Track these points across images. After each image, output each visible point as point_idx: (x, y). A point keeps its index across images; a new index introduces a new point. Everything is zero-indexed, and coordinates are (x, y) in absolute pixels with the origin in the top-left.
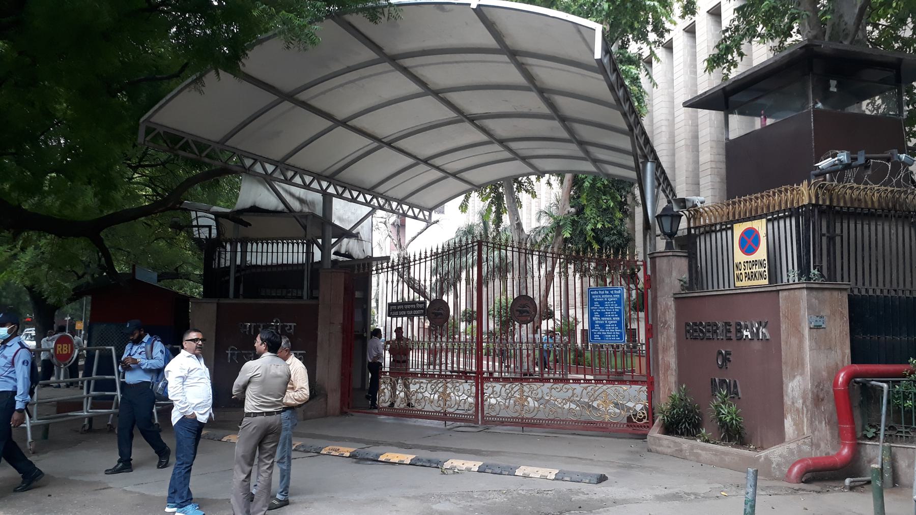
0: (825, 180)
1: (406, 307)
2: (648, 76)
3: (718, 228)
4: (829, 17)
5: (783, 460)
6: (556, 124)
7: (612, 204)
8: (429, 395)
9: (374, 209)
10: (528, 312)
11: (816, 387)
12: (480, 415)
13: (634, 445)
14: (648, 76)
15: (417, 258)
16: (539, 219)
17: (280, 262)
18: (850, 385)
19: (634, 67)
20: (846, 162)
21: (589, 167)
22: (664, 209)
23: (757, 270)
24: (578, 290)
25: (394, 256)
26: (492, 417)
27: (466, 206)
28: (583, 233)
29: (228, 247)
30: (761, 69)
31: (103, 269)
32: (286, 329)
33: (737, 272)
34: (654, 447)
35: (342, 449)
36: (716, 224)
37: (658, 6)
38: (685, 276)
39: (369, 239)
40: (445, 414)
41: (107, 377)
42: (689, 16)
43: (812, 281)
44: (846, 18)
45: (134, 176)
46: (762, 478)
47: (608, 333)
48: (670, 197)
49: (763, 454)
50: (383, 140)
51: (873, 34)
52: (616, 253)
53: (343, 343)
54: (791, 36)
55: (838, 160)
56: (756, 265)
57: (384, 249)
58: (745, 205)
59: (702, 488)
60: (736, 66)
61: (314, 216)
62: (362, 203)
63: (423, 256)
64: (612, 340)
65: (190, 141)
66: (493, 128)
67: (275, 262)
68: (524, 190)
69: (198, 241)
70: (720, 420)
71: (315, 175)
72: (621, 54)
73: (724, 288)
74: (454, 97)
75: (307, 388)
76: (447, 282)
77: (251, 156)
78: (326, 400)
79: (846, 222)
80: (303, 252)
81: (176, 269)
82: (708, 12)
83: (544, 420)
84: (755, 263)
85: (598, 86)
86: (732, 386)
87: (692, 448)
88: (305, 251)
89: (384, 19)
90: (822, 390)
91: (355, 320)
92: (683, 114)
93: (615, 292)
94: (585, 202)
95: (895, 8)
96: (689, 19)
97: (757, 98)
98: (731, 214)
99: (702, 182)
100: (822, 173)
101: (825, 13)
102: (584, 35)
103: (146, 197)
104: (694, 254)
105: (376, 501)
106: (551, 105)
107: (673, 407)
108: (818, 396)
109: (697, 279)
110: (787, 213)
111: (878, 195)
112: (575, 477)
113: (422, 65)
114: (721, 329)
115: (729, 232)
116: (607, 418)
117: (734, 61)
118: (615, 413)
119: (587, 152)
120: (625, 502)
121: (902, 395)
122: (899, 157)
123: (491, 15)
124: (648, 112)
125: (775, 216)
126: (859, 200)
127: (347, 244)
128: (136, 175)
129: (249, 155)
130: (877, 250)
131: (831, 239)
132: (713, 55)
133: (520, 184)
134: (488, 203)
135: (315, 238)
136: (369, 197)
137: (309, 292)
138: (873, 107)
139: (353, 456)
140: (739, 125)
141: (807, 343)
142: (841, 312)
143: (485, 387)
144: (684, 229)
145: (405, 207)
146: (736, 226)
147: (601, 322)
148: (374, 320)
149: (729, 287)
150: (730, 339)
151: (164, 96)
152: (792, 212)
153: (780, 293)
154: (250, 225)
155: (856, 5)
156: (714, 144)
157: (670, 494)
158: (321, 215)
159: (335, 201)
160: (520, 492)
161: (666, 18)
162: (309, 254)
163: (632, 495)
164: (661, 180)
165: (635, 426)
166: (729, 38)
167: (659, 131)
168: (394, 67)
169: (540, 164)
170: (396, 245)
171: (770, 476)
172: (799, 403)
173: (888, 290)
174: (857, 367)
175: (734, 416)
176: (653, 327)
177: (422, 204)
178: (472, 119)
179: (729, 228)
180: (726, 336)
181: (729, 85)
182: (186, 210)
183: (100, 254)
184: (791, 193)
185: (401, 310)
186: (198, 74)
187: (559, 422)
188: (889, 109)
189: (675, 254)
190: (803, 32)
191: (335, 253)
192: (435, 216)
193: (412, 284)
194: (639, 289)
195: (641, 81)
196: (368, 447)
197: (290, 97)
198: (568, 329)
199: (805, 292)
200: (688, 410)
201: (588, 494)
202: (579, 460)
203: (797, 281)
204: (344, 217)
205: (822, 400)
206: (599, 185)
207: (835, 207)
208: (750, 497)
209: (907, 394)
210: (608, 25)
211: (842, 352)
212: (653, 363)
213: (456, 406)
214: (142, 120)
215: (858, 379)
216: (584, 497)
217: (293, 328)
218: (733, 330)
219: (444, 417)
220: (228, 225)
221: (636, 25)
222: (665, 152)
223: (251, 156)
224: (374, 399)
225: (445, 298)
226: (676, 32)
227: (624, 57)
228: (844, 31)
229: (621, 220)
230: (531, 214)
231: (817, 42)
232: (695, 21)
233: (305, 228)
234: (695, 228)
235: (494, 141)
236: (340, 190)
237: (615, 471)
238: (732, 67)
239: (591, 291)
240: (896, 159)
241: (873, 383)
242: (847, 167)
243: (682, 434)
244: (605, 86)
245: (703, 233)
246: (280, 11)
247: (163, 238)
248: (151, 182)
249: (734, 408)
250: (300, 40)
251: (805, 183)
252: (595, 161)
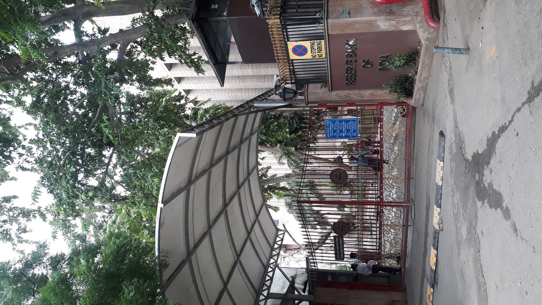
0: (266, 11)
1: (338, 248)
2: (204, 104)
3: (291, 67)
5: (427, 31)
6: (230, 157)
12: (403, 204)
13: (419, 114)
14: (204, 104)
15: (306, 233)
16: (283, 164)
19: (199, 112)
21: (254, 138)
23: (316, 46)
26: (405, 197)
27: (275, 207)
33: (317, 57)
34: (420, 102)
35: (428, 293)
36: (290, 69)
38: (319, 85)
39: (295, 270)
40: (404, 226)
43: (323, 16)
46: (437, 42)
47: (352, 128)
49: (423, 42)
50: (236, 260)
55: (256, 4)
57: (300, 259)
58: (279, 53)
59: (445, 76)
62: (273, 274)
64: (356, 126)
74: (212, 216)
83: (405, 166)
84: (312, 48)
85: (210, 136)
86: (384, 59)
87: (420, 81)
90: (385, 10)
91: (346, 281)
93: (328, 123)
97: (220, 47)
100: (263, 12)
101: (174, 10)
102: (182, 143)
104: (306, 81)
105: (462, 274)
107: (396, 91)
108: (389, 13)
109: (320, 79)
110: (284, 31)
112: (441, 150)
113: (194, 236)
114: (349, 66)
115: (294, 61)
116: (403, 129)
117: (198, 58)
118: (400, 124)
120: (455, 121)
124: (224, 104)
125: (286, 37)
127: (298, 285)
131: (299, 7)
132: (195, 70)
136: (270, 269)
139: (433, 286)
140: (234, 55)
141: (358, 19)
143: (387, 201)
145: (276, 246)
146: (291, 58)
149: (326, 61)
150: (356, 61)
152: (284, 28)
153: (330, 33)
157: (450, 95)
158: (280, 301)
159: (272, 291)
160: (452, 183)
163: (451, 117)
164: (264, 98)
165: (408, 113)
166: (185, 61)
167: (234, 97)
168: (194, 253)
169: (252, 164)
170: (298, 251)
171: (436, 39)
176: (348, 102)
177: (274, 235)
178: (226, 205)
179: (292, 62)
180: (354, 57)
184: (273, 28)
185: (340, 252)
187: (407, 157)
189: (306, 91)
190: (184, 22)
192: (280, 227)
193: (322, 242)
196: (427, 276)
198: (348, 148)
199: (329, 20)
200: (398, 84)
201: (452, 143)
202: (430, 146)
203: (323, 25)
204: (282, 286)
205: (391, 10)
206: (264, 131)
207: (281, 5)
208: (450, 51)
216: (454, 145)
218: (350, 59)
219: (406, 226)
221: (176, 111)
226: (179, 88)
230: (280, 169)
231: (191, 16)
232: (174, 78)
234: (291, 80)
235: (238, 192)
236: (265, 287)
237: (436, 126)
238: (202, 59)
239: (327, 137)
243: (412, 86)
245: (295, 76)
251: (267, 21)
252: (252, 134)
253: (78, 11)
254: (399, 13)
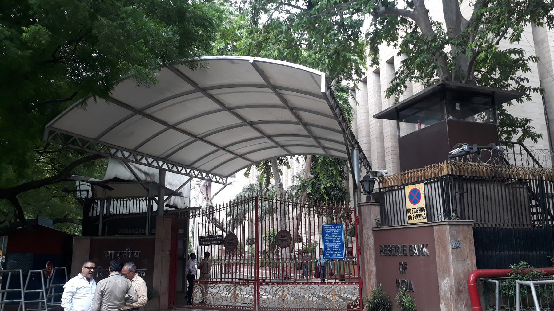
0: (456, 161)
1: (211, 239)
2: (353, 99)
3: (396, 188)
4: (453, 68)
6: (301, 127)
7: (335, 172)
8: (224, 295)
9: (192, 177)
10: (286, 241)
11: (458, 283)
12: (257, 306)
14: (353, 99)
16: (293, 182)
17: (131, 212)
18: (477, 282)
19: (345, 94)
20: (467, 150)
21: (320, 151)
22: (365, 177)
23: (420, 213)
24: (316, 224)
25: (204, 206)
26: (264, 308)
27: (248, 174)
28: (318, 189)
29: (99, 203)
30: (417, 97)
31: (17, 217)
32: (134, 254)
33: (409, 215)
37: (358, 59)
38: (379, 217)
41: (16, 290)
42: (376, 65)
44: (463, 68)
45: (41, 158)
47: (335, 253)
48: (368, 169)
50: (197, 136)
51: (478, 76)
52: (338, 203)
53: (170, 263)
54: (433, 77)
55: (462, 149)
56: (419, 210)
57: (198, 200)
60: (402, 93)
61: (153, 183)
62: (184, 174)
63: (221, 207)
64: (337, 257)
65: (77, 139)
66: (264, 129)
67: (128, 212)
68: (284, 164)
69: (80, 200)
70: (403, 305)
71: (155, 158)
72: (337, 86)
73: (401, 224)
74: (240, 112)
75: (146, 295)
76: (237, 221)
77: (115, 147)
78: (159, 300)
79: (469, 184)
80: (146, 206)
81: (65, 216)
82: (387, 62)
84: (418, 209)
88: (147, 205)
89: (198, 69)
90: (461, 285)
92: (374, 122)
93: (338, 227)
94: (319, 171)
95: (489, 63)
96: (375, 67)
97: (415, 113)
98: (403, 180)
99: (386, 159)
100: (454, 157)
101: (451, 65)
102: (315, 79)
103: (48, 171)
106: (298, 117)
107: (375, 298)
109: (385, 218)
110: (435, 180)
111: (486, 169)
113: (222, 94)
115: (403, 191)
116: (335, 306)
117: (401, 91)
118: (340, 303)
119: (319, 143)
121: (507, 287)
122: (496, 147)
123: (260, 66)
125: (428, 181)
126: (476, 172)
127: (174, 200)
128: (42, 157)
129: (113, 146)
130: (487, 201)
131: (461, 195)
133: (281, 161)
134: (262, 172)
135: (153, 197)
136: (188, 170)
137: (149, 230)
138: (481, 117)
141: (451, 257)
142: (469, 238)
143: (260, 289)
144: (377, 189)
146: (407, 187)
147: (330, 246)
148: (191, 246)
150: (406, 255)
151: (62, 111)
153: (434, 227)
154: (113, 189)
155: (468, 60)
156: (392, 137)
158: (158, 182)
159: (167, 173)
161: (363, 66)
162: (150, 206)
164: (363, 160)
166: (398, 78)
169: (293, 149)
170: (205, 198)
172: (448, 294)
173: (495, 224)
174: (481, 271)
175: (411, 303)
176: (362, 248)
177: (221, 173)
178: (251, 124)
179: (403, 188)
181: (399, 106)
182: (73, 180)
183: (15, 208)
184: (437, 168)
185: (207, 241)
186: (83, 99)
188: (490, 118)
189: (372, 204)
191: (166, 206)
192: (230, 180)
193: (215, 222)
194: (352, 225)
195: (349, 101)
197: (141, 112)
198: (311, 249)
199: (448, 227)
203: (443, 220)
204: (173, 183)
205: (462, 292)
206: (327, 161)
207: (462, 176)
209: (510, 287)
210: (329, 72)
212: (362, 271)
213: (242, 302)
214: (47, 126)
215: (481, 279)
217: (138, 253)
218: (408, 249)
220: (99, 189)
221: (346, 70)
222: (365, 142)
223: (115, 147)
224: (190, 298)
225: (235, 232)
226: (369, 72)
227: (339, 88)
228: (462, 75)
229: (341, 181)
231: (447, 82)
233: (148, 190)
234: (383, 188)
235: (264, 136)
236: (170, 166)
238: (400, 94)
239: (324, 227)
240: (494, 148)
241: (490, 280)
242: (468, 153)
244: (327, 106)
245: (387, 191)
246: (134, 65)
247: (58, 197)
248: (51, 162)
249: (410, 298)
250: (147, 81)
251: (445, 162)
252: (324, 148)
254: (459, 300)
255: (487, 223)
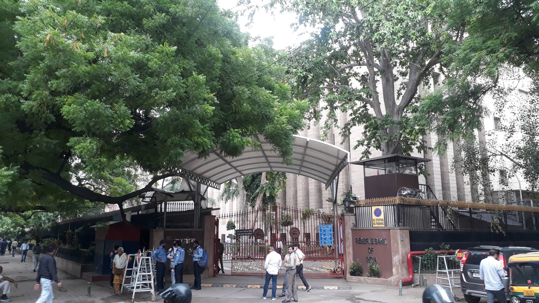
1: (244, 231)
49: (389, 279)
59: (380, 289)
84: (380, 219)
87: (364, 279)
141: (400, 245)
146: (373, 207)
150: (373, 244)
163: (363, 291)
185: (242, 233)
211: (408, 247)
218: (374, 241)
253: (390, 74)
255: (414, 228)
